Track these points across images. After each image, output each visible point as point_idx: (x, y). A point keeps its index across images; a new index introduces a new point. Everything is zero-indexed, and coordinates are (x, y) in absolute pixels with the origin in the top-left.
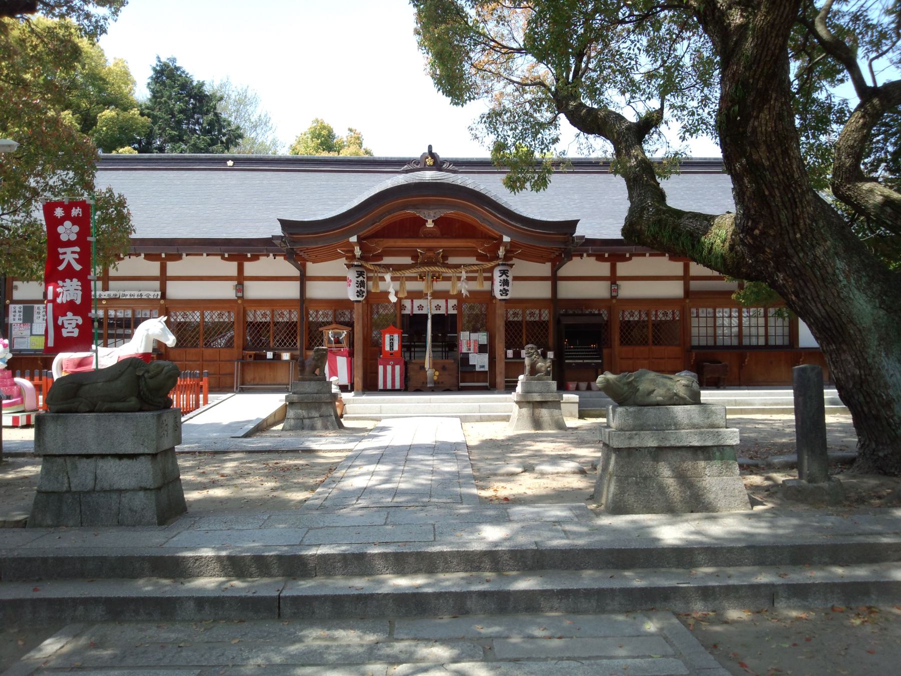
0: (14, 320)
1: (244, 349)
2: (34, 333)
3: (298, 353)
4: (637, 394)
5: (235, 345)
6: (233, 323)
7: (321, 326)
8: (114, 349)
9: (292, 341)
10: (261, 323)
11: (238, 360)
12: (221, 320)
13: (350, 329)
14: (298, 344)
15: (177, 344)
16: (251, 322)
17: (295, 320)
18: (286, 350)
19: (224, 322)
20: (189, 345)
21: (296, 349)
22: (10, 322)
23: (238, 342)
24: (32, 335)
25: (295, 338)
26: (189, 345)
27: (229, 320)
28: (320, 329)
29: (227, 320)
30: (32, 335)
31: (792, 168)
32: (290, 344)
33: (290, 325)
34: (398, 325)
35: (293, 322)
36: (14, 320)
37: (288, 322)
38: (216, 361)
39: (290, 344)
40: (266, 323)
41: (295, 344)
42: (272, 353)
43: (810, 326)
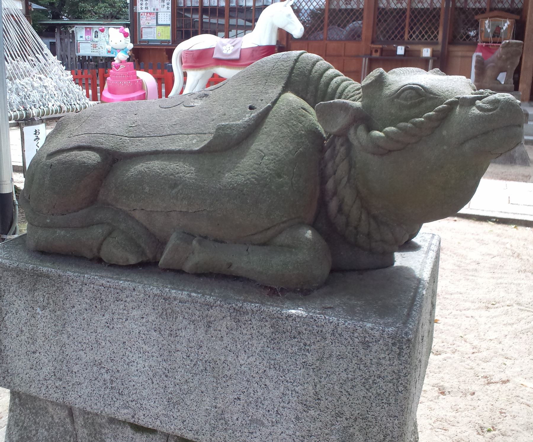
0: (141, 8)
1: (373, 42)
2: (159, 23)
3: (439, 48)
4: (112, 63)
5: (363, 37)
6: (363, 10)
7: (477, 14)
8: (235, 39)
9: (433, 33)
10: (395, 9)
11: (365, 56)
12: (349, 7)
13: (518, 17)
14: (440, 37)
15: (304, 36)
16: (383, 9)
17: (438, 5)
18: (427, 44)
19: (352, 10)
20: (395, 14)
21: (437, 44)
22: (138, 11)
23: (367, 33)
24: (157, 24)
25: (436, 28)
26: (395, 14)
27: (358, 6)
28: (476, 17)
29: (355, 7)
30: (157, 24)
31: (348, 22)
32: (429, 36)
33: (431, 13)
34: (505, 20)
35: (435, 9)
36: (141, 8)
37: (428, 9)
38: (341, 56)
39: (429, 36)
40: (401, 9)
41: (435, 37)
42: (403, 48)
43: (146, 70)
